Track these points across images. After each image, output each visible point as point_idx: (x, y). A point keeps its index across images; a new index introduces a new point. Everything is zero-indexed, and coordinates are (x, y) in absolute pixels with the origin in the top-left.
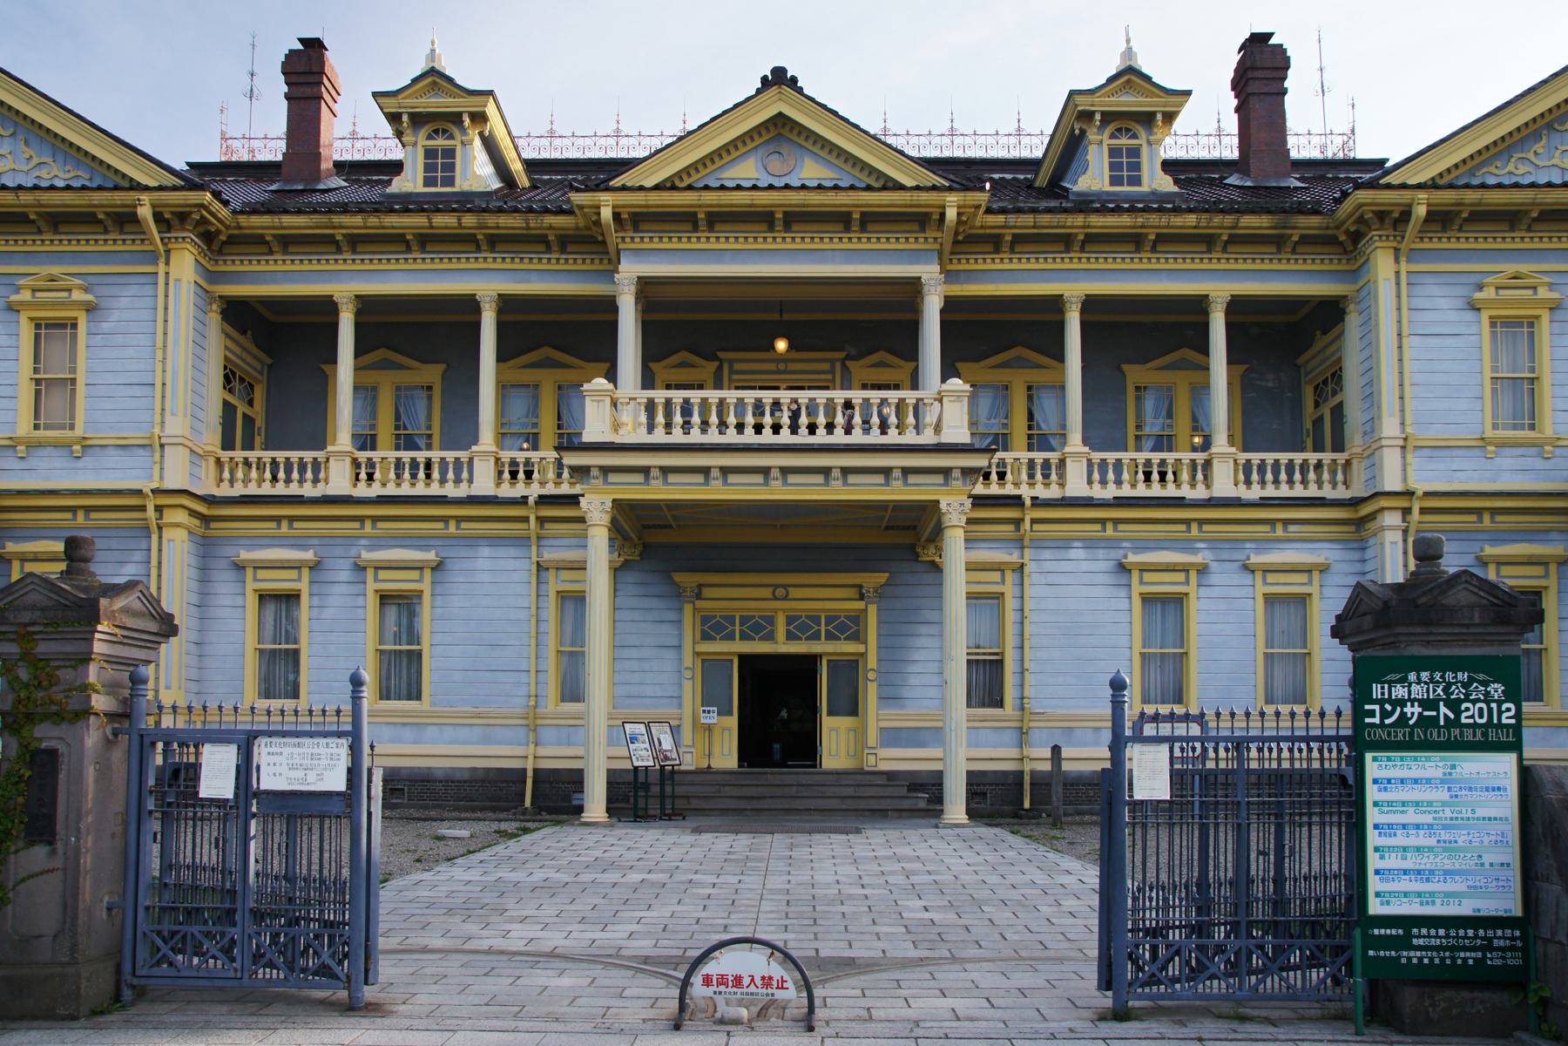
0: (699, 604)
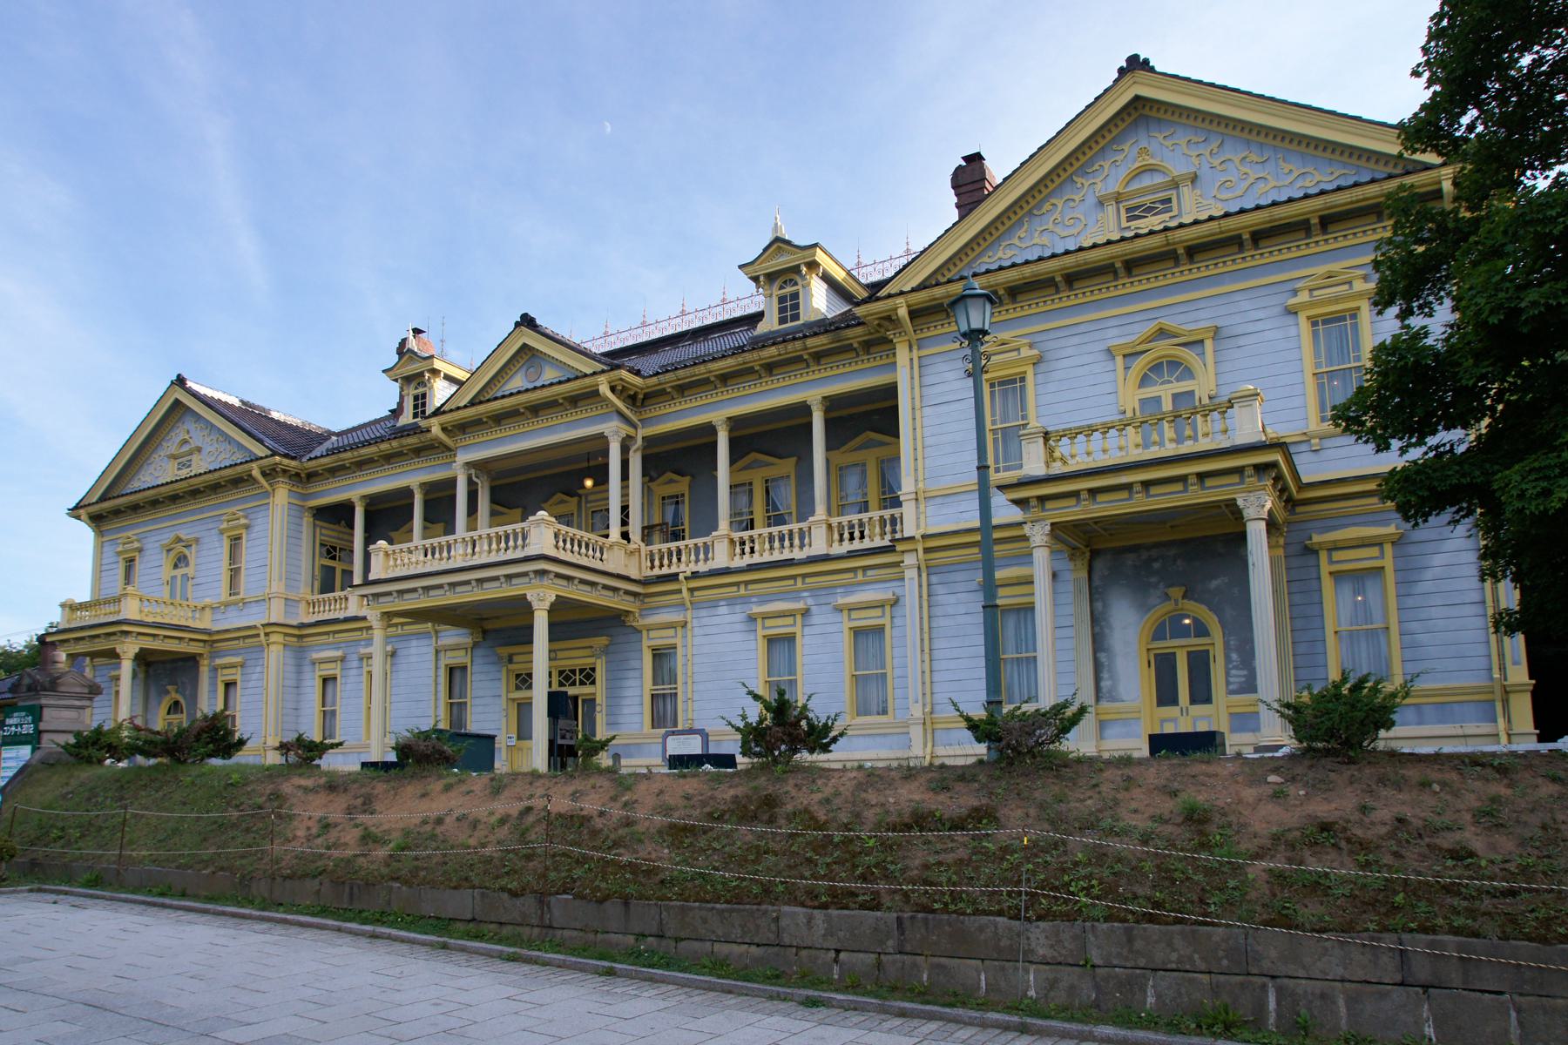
0: (511, 667)
